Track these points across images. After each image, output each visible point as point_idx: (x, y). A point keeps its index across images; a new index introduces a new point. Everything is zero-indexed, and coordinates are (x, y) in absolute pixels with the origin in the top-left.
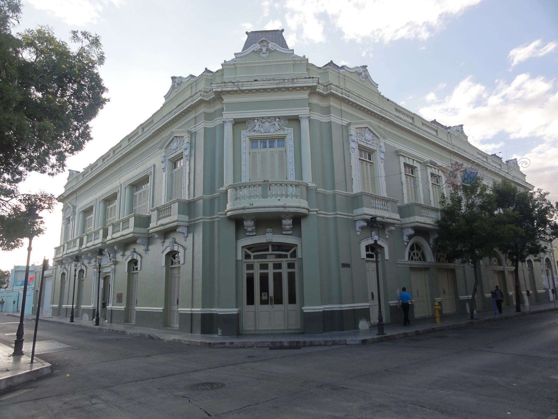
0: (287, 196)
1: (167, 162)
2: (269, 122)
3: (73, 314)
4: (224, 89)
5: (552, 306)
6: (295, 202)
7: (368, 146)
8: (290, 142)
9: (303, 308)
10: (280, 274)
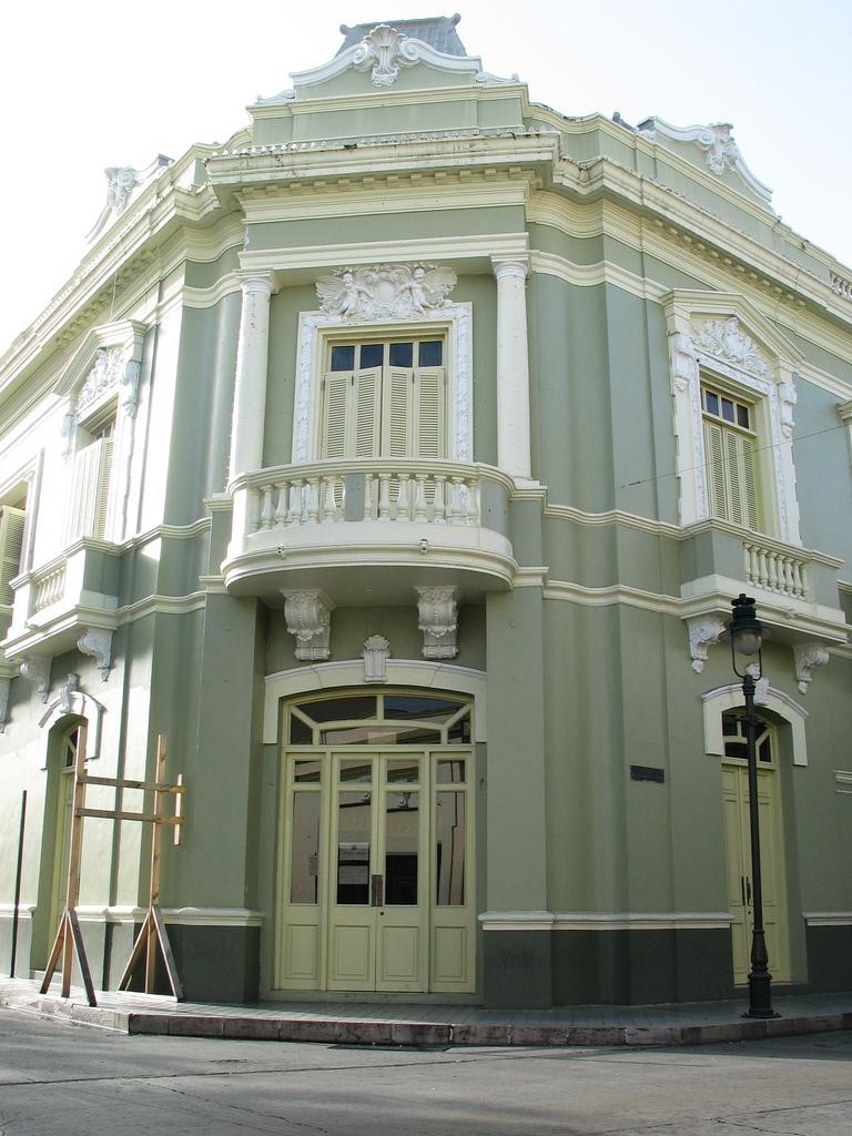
4: (246, 179)
6: (464, 538)
7: (738, 377)
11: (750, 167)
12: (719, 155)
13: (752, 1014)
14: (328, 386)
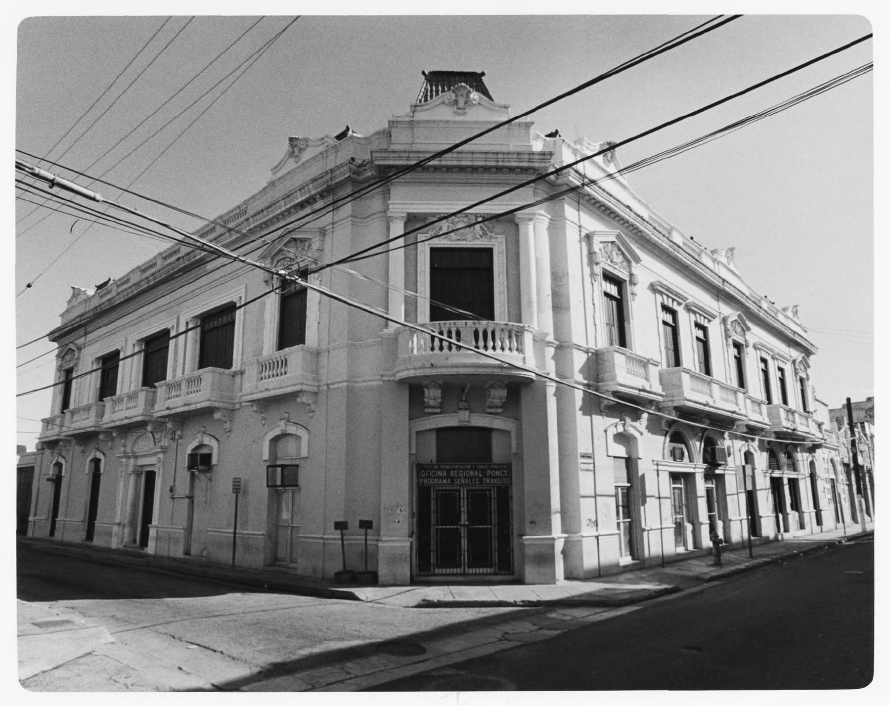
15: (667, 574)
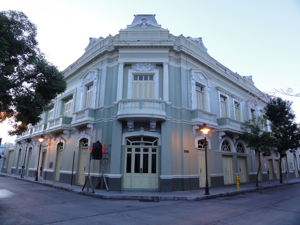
0: (154, 108)
1: (84, 87)
2: (145, 66)
3: (22, 173)
4: (120, 45)
5: (297, 180)
7: (201, 83)
8: (156, 77)
9: (160, 176)
10: (147, 155)
11: (205, 46)
12: (200, 43)
13: (206, 194)
14: (133, 83)
15: (32, 190)
